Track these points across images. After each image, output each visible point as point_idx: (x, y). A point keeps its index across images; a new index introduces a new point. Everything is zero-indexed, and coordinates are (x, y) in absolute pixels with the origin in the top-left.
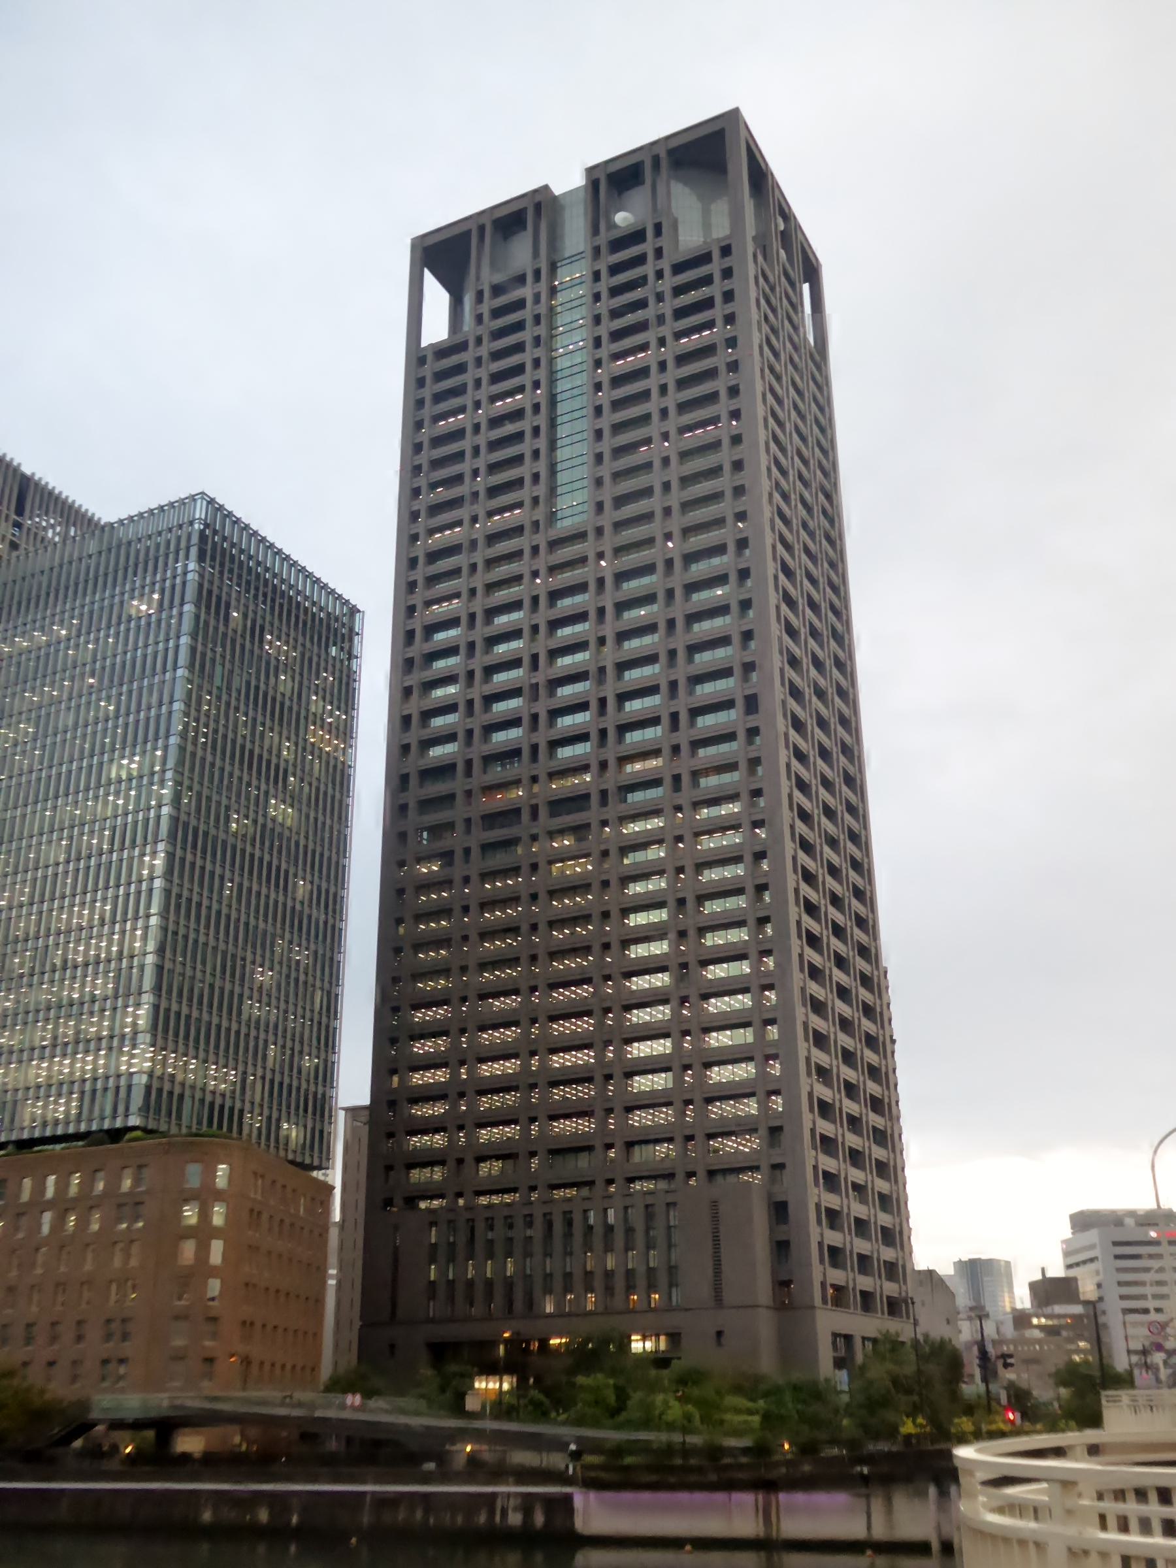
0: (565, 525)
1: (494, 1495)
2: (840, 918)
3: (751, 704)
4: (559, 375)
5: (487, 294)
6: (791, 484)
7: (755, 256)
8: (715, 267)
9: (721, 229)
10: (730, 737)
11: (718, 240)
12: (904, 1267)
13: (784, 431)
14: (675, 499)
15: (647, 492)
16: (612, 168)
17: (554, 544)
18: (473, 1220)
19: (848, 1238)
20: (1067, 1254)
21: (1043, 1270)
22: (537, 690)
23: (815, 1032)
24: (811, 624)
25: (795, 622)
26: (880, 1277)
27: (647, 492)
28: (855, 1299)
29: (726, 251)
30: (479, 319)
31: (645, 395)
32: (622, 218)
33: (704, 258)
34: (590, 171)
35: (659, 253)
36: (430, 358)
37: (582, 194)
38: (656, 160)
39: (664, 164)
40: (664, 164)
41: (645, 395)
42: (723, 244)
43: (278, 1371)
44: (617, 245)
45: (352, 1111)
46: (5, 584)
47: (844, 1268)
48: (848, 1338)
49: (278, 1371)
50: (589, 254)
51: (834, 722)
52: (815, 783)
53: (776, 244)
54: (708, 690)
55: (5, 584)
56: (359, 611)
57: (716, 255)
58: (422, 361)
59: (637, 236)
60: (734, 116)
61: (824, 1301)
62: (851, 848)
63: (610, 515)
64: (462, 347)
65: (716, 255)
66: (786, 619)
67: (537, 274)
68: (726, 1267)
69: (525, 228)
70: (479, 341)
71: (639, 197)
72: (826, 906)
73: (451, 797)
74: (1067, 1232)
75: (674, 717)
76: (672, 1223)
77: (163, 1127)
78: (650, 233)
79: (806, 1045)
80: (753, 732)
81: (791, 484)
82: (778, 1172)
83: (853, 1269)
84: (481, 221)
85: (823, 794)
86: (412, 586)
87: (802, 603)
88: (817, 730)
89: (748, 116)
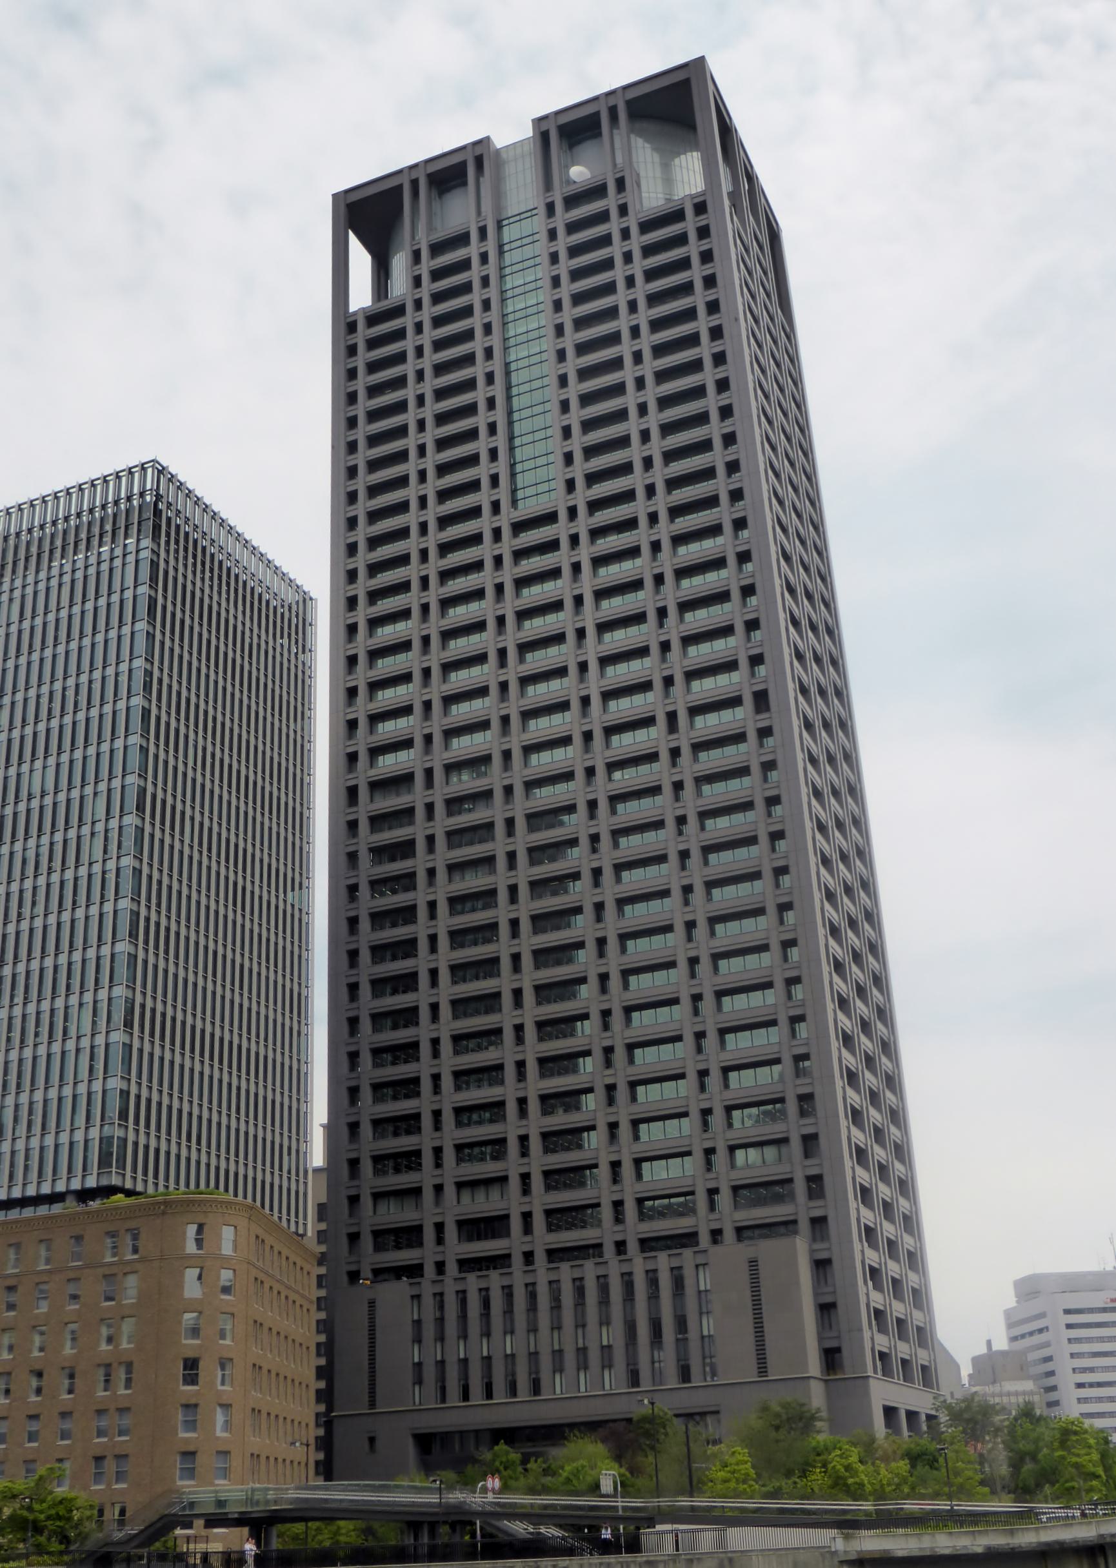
0: (529, 508)
5: (425, 254)
8: (690, 224)
10: (740, 738)
11: (692, 197)
18: (487, 1289)
20: (1010, 1326)
21: (989, 1343)
30: (417, 281)
32: (579, 173)
33: (678, 215)
34: (539, 122)
35: (623, 210)
36: (361, 325)
37: (526, 148)
38: (613, 112)
43: (280, 1465)
44: (571, 201)
45: (317, 1171)
46: (6, 539)
49: (280, 1465)
50: (542, 210)
55: (6, 539)
56: (311, 599)
57: (689, 212)
58: (352, 327)
59: (597, 191)
60: (700, 63)
65: (689, 212)
67: (483, 232)
69: (465, 184)
70: (418, 304)
71: (588, 149)
73: (410, 812)
74: (1011, 1301)
76: (702, 1288)
77: (140, 1187)
78: (611, 188)
84: (611, 103)
89: (716, 67)
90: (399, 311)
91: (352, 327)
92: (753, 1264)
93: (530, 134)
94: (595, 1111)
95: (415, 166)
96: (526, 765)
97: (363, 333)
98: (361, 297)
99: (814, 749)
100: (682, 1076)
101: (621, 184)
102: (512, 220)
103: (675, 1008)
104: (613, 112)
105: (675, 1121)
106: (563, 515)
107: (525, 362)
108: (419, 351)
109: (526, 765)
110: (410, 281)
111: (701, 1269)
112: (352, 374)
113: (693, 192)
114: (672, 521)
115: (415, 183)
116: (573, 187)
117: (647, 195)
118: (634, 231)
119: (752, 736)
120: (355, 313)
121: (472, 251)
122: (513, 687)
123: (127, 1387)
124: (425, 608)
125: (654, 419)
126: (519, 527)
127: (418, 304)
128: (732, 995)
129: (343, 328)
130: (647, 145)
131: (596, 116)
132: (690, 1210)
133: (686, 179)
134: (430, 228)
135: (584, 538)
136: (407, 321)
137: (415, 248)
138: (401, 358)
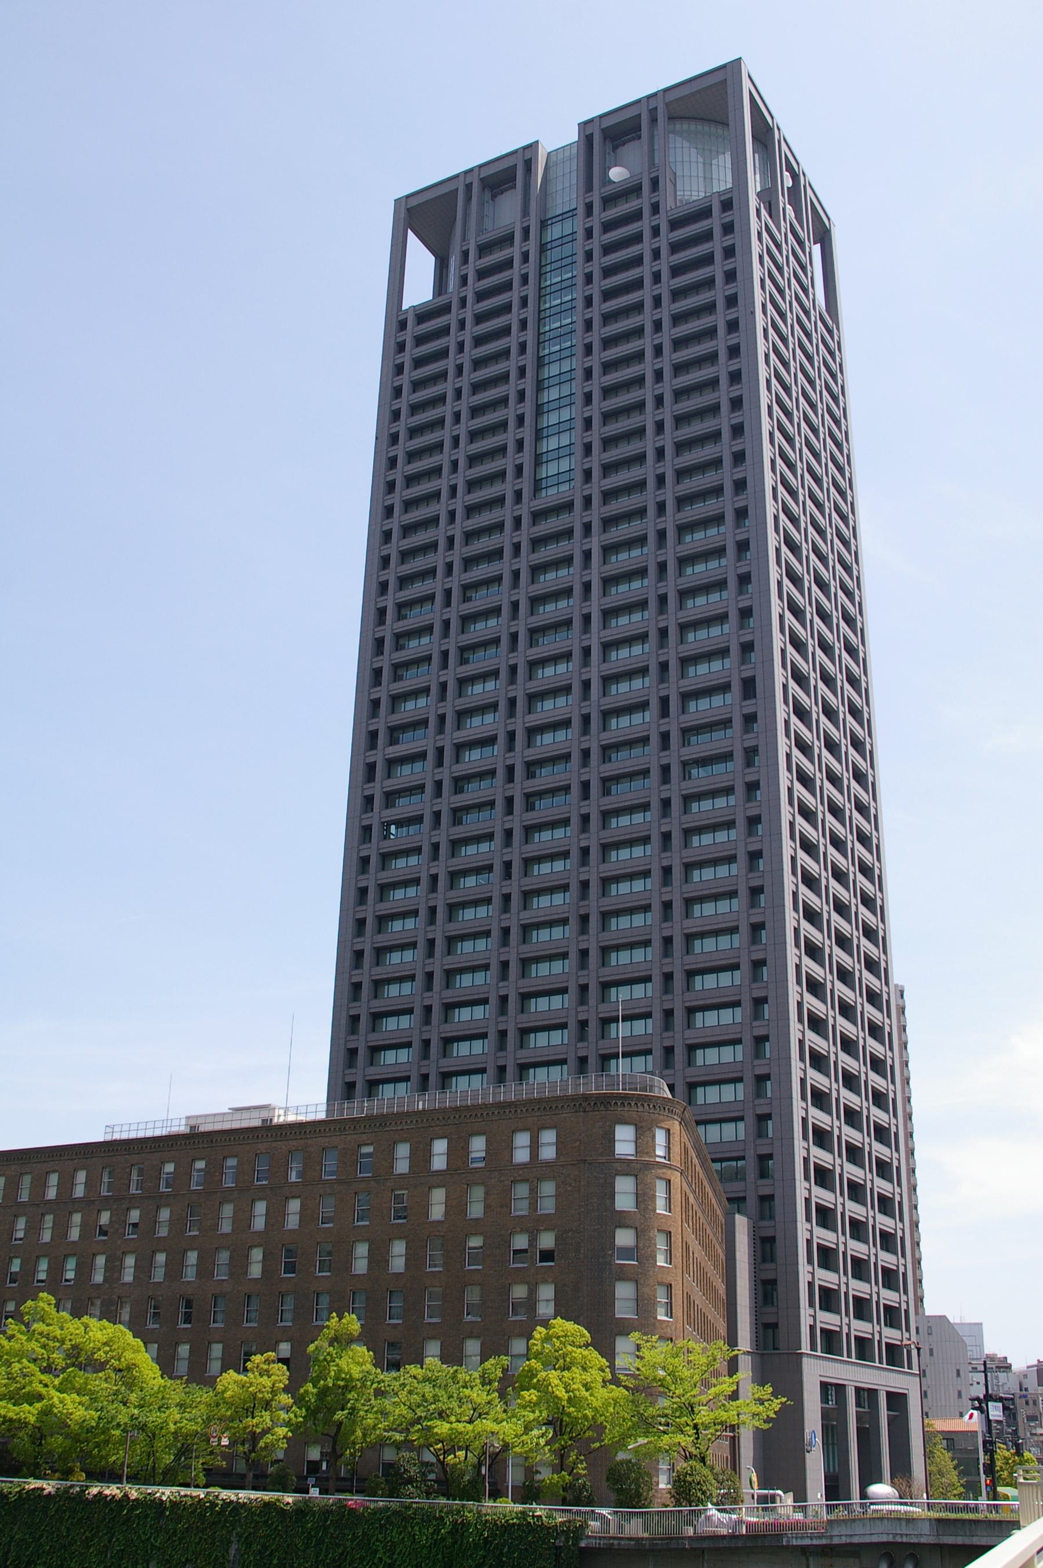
0: (551, 496)
1: (682, 1511)
2: (845, 927)
3: (749, 687)
6: (807, 566)
7: (758, 211)
8: (715, 222)
9: (723, 181)
13: (784, 299)
15: (640, 458)
16: (607, 123)
17: (537, 516)
22: (516, 673)
25: (803, 666)
27: (640, 458)
29: (727, 205)
30: (464, 280)
32: (617, 174)
33: (705, 213)
34: (584, 126)
35: (655, 208)
37: (574, 151)
38: (653, 113)
44: (608, 201)
47: (838, 1312)
48: (840, 1388)
50: (581, 211)
52: (819, 777)
53: (783, 201)
54: (703, 672)
58: (403, 325)
59: (632, 190)
61: (813, 1347)
63: (598, 485)
64: (446, 309)
67: (526, 231)
69: (514, 187)
70: (463, 302)
71: (634, 152)
72: (829, 913)
75: (665, 701)
93: (575, 138)
95: (471, 170)
97: (413, 329)
99: (806, 735)
101: (655, 183)
104: (653, 113)
106: (578, 504)
115: (469, 187)
117: (682, 193)
118: (664, 228)
121: (515, 251)
123: (188, 1320)
124: (662, 535)
126: (537, 516)
127: (463, 302)
128: (631, 984)
130: (686, 144)
134: (481, 230)
136: (451, 319)
137: (464, 248)
138: (637, 284)
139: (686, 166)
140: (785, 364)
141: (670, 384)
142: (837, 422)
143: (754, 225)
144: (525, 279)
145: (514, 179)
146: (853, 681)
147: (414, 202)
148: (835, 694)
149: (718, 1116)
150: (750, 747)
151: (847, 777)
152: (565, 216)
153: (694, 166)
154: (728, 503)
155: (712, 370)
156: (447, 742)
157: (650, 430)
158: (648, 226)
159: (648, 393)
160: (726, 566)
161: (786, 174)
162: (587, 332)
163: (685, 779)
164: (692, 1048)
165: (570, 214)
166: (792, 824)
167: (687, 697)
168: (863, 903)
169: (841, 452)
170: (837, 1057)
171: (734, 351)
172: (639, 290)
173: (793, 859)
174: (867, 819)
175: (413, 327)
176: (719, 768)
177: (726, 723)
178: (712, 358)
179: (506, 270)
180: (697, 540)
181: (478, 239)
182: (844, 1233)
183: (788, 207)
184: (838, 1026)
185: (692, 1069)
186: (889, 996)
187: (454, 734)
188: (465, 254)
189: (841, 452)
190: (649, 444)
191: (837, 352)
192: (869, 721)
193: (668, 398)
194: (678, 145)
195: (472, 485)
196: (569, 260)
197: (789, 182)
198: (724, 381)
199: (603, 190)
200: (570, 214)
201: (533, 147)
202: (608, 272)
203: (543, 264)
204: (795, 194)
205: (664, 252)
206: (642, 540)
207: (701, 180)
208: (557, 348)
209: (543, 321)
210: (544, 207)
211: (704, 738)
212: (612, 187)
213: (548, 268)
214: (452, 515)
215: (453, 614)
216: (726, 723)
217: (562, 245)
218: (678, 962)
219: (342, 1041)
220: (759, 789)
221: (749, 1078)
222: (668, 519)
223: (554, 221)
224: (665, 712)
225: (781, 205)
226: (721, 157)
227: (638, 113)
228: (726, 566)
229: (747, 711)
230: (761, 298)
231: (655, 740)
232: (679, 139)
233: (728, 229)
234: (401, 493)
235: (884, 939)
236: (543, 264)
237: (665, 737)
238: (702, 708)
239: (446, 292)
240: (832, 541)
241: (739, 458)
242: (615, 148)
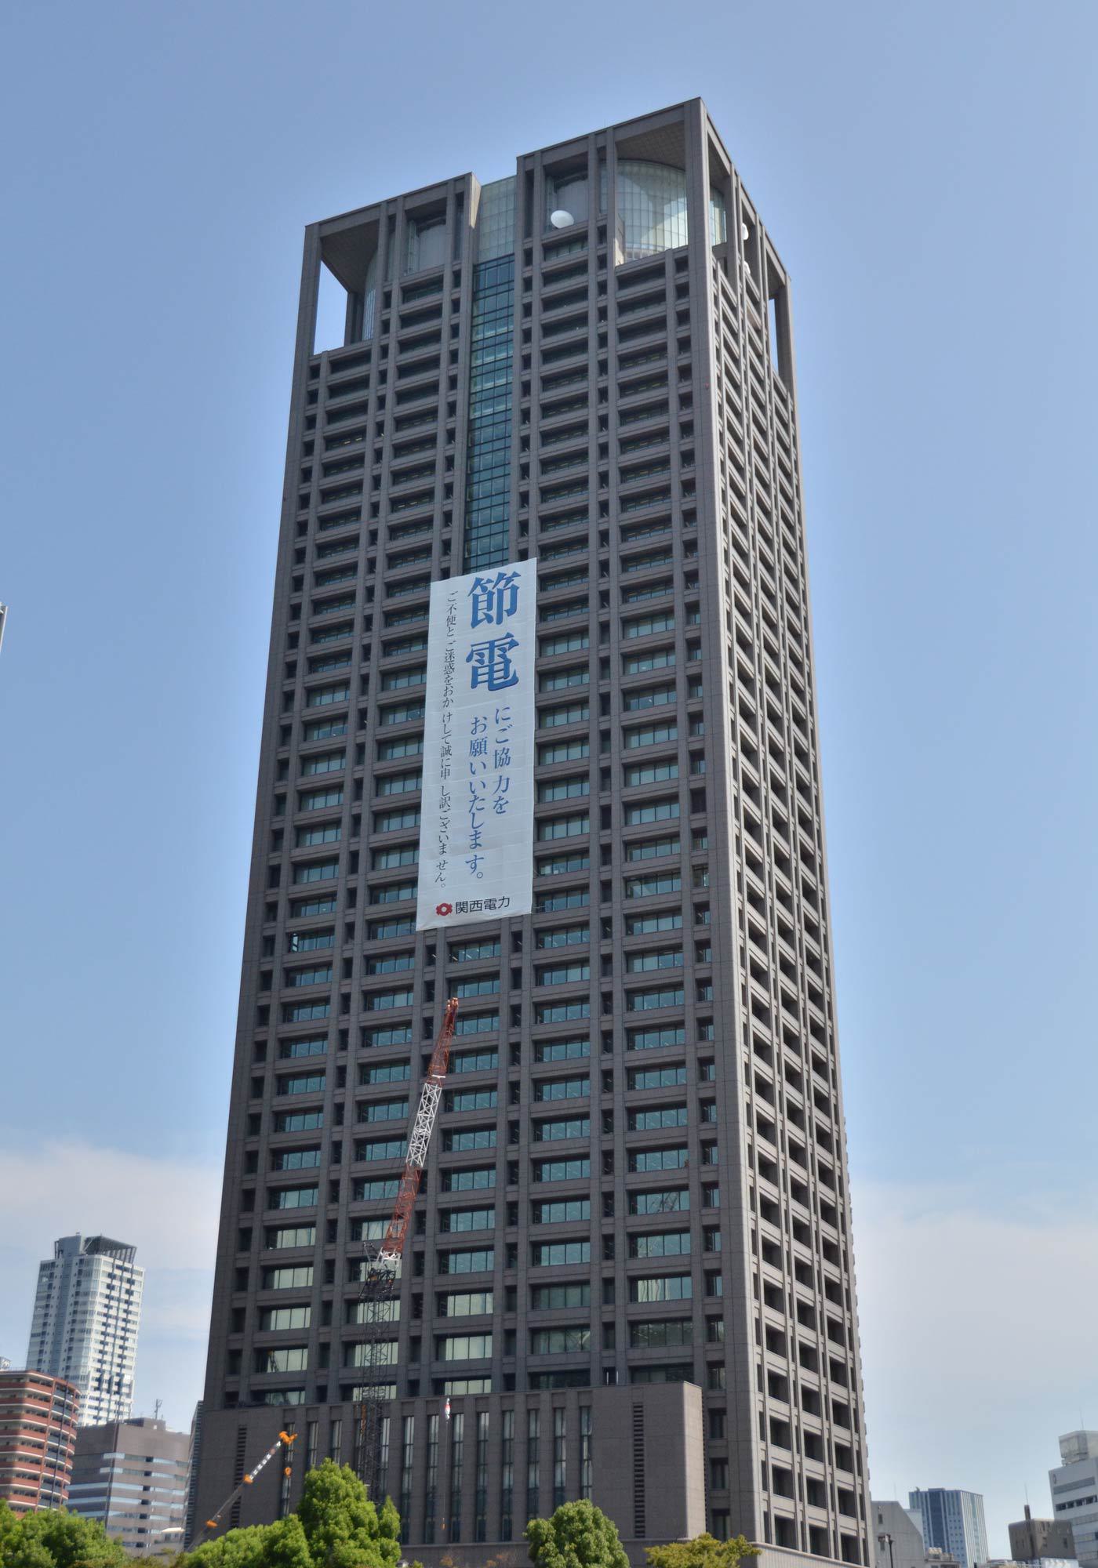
3: (698, 799)
4: (481, 295)
6: (754, 544)
7: (715, 272)
8: (669, 282)
12: (862, 1497)
13: (737, 342)
14: (615, 550)
19: (800, 1507)
21: (1027, 1510)
23: (761, 1158)
24: (769, 704)
26: (833, 1509)
28: (803, 1537)
30: (385, 326)
31: (582, 427)
32: (560, 218)
34: (523, 160)
36: (324, 370)
37: (511, 186)
38: (601, 151)
39: (611, 155)
40: (611, 155)
41: (581, 372)
42: (678, 256)
44: (550, 249)
51: (791, 788)
54: (647, 781)
57: (670, 268)
58: (315, 372)
59: (576, 238)
61: (768, 1540)
62: (814, 1044)
65: (670, 268)
66: (739, 663)
67: (457, 275)
68: (649, 1492)
69: (444, 222)
70: (384, 351)
71: (576, 192)
75: (606, 811)
79: (756, 1303)
80: (699, 834)
81: (754, 544)
82: (720, 1518)
83: (801, 1499)
84: (391, 211)
85: (783, 980)
86: (291, 669)
87: (760, 681)
88: (774, 832)
90: (364, 357)
91: (315, 372)
92: (638, 1409)
94: (494, 1229)
96: (626, 824)
97: (326, 378)
98: (331, 336)
100: (585, 1197)
102: (488, 265)
103: (682, 1111)
104: (601, 151)
105: (676, 1237)
107: (489, 421)
108: (603, 340)
109: (626, 824)
110: (378, 324)
111: (508, 1415)
112: (311, 422)
113: (675, 246)
114: (625, 601)
115: (392, 219)
116: (554, 233)
119: (686, 837)
120: (320, 356)
121: (445, 297)
122: (616, 737)
124: (605, 627)
125: (615, 491)
127: (384, 351)
129: (306, 372)
130: (636, 189)
131: (442, 203)
132: (686, 1337)
133: (674, 230)
135: (615, 595)
136: (372, 369)
137: (386, 289)
138: (582, 320)
139: (636, 215)
140: (736, 361)
141: (617, 460)
142: (785, 426)
143: (711, 288)
144: (455, 331)
145: (443, 212)
146: (799, 721)
147: (328, 231)
148: (780, 700)
149: (660, 1227)
150: (698, 865)
151: (797, 896)
152: (501, 262)
153: (644, 214)
154: (677, 596)
155: (664, 568)
156: (363, 846)
157: (593, 510)
158: (595, 657)
159: (591, 468)
160: (673, 629)
161: (744, 226)
162: (524, 423)
163: (626, 860)
164: (632, 1112)
165: (506, 260)
166: (741, 912)
167: (629, 807)
168: (817, 1105)
169: (786, 407)
170: (792, 1288)
171: (684, 344)
172: (582, 274)
173: (744, 988)
174: (817, 940)
175: (316, 507)
176: (664, 886)
177: (673, 837)
178: (661, 378)
179: (432, 292)
180: (644, 635)
181: (544, 237)
182: (796, 1405)
183: (745, 264)
184: (784, 1093)
185: (632, 1093)
186: (844, 1209)
187: (367, 909)
188: (387, 297)
189: (786, 407)
190: (592, 526)
191: (791, 424)
192: (821, 866)
193: (382, 535)
194: (628, 190)
195: (395, 531)
196: (504, 313)
197: (745, 235)
198: (674, 432)
199: (544, 237)
200: (506, 260)
201: (465, 179)
202: (549, 304)
203: (475, 314)
204: (751, 245)
205: (612, 312)
206: (582, 632)
207: (651, 214)
208: (489, 411)
209: (475, 354)
210: (476, 250)
211: (648, 852)
212: (554, 233)
213: (480, 320)
214: (373, 535)
215: (369, 737)
216: (673, 837)
217: (496, 320)
218: (618, 1098)
219: (281, 656)
220: (701, 684)
221: (696, 1228)
222: (614, 907)
223: (488, 265)
224: (606, 823)
225: (738, 262)
226: (673, 203)
227: (585, 151)
228: (673, 629)
229: (696, 825)
230: (719, 427)
231: (595, 853)
232: (628, 182)
233: (682, 291)
234: (305, 648)
235: (832, 1037)
236: (475, 314)
237: (606, 850)
238: (646, 820)
239: (360, 339)
240: (779, 551)
241: (689, 516)
242: (557, 188)
